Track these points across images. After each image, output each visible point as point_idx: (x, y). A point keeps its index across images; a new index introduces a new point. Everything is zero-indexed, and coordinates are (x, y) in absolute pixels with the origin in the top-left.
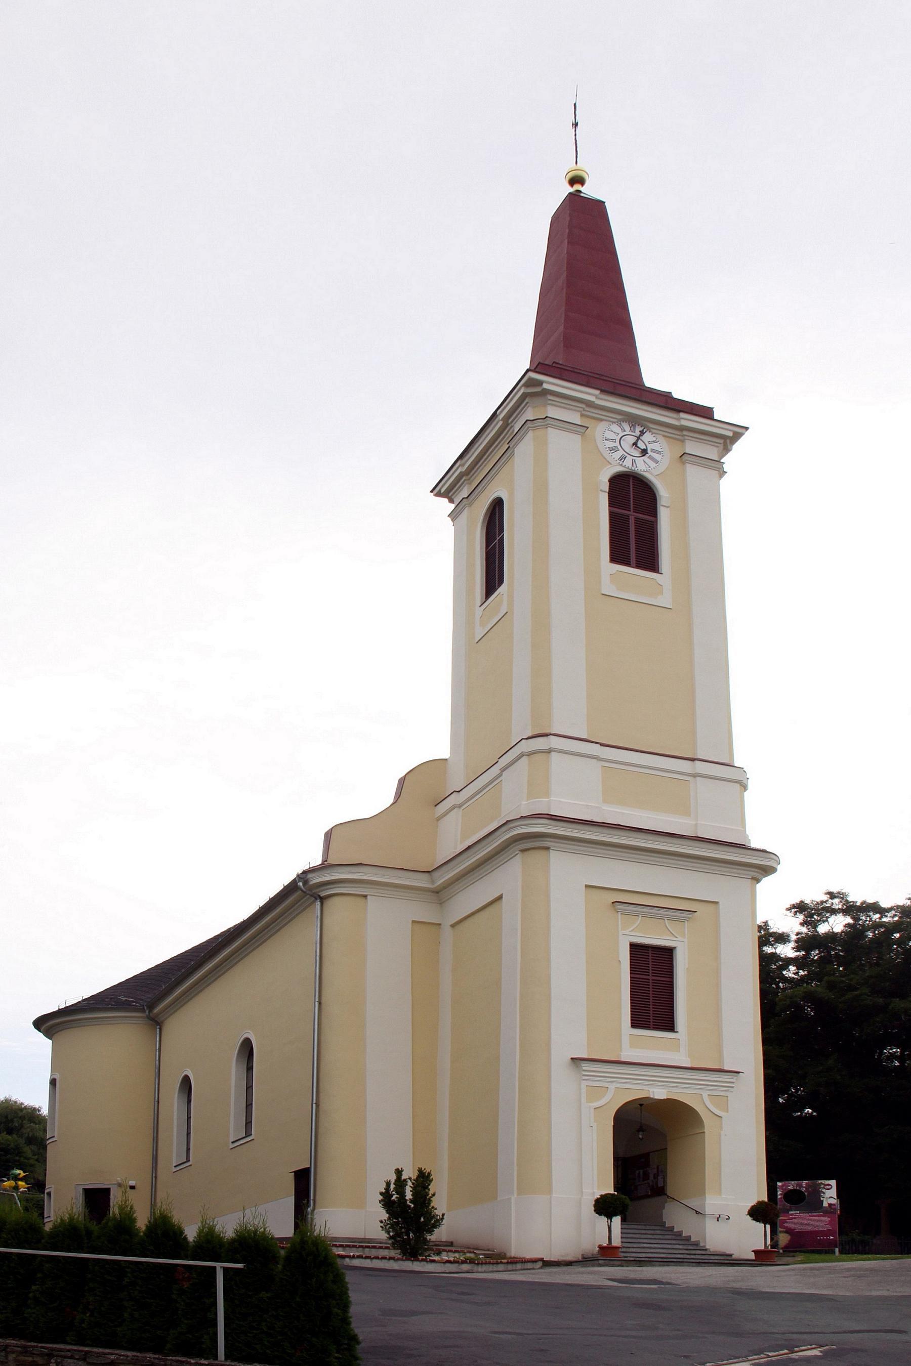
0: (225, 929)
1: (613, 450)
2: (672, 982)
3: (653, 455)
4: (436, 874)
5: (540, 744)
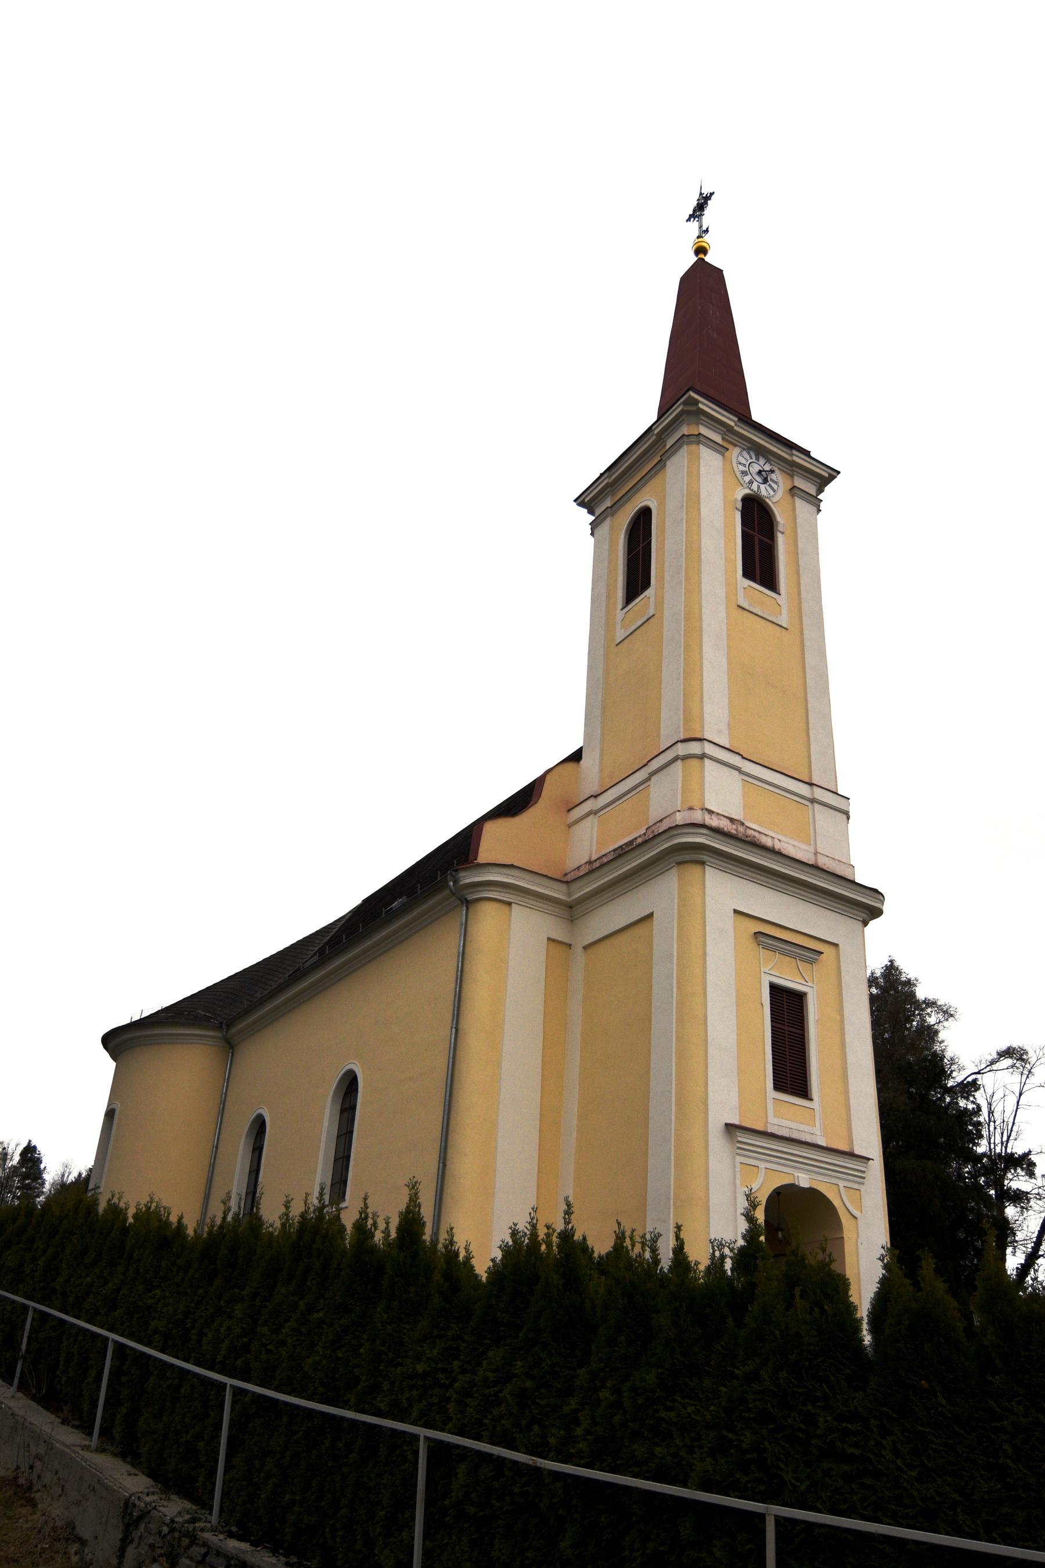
0: (301, 938)
2: (803, 1035)
4: (574, 886)
5: (694, 748)
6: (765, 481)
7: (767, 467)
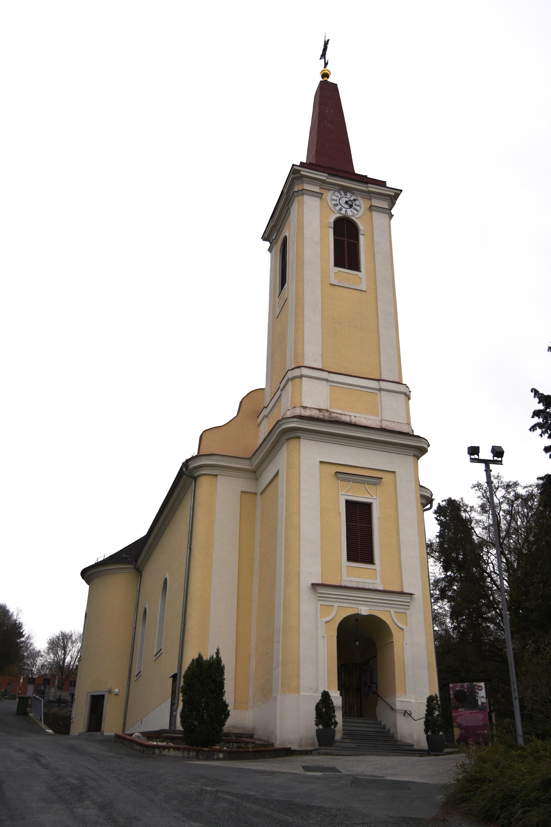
1: (336, 205)
3: (356, 207)
4: (253, 460)
5: (297, 372)
6: (351, 206)
7: (352, 198)
